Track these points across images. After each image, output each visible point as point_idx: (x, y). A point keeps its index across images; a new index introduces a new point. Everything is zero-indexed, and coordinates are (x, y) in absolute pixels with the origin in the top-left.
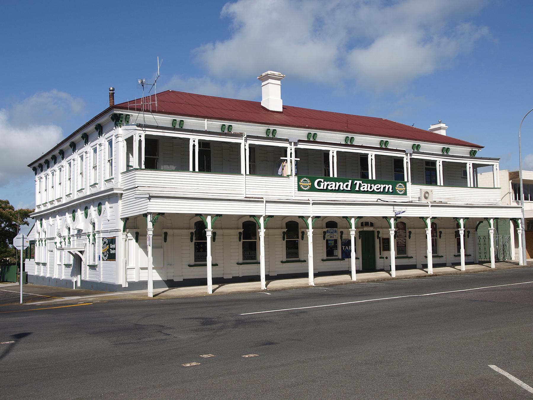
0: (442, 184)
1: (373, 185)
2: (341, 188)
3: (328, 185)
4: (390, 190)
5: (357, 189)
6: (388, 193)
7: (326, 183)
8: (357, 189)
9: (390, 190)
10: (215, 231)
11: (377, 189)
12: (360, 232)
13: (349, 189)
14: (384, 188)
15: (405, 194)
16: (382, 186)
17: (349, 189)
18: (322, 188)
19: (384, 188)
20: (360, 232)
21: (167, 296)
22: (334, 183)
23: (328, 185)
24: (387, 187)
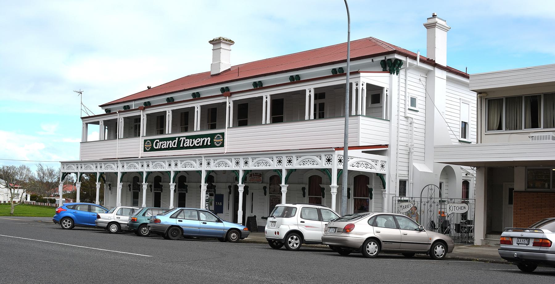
0: (365, 115)
1: (194, 140)
2: (171, 147)
3: (162, 144)
4: (209, 144)
5: (181, 146)
6: (207, 146)
7: (161, 143)
8: (181, 146)
9: (209, 144)
10: (247, 184)
11: (198, 143)
12: (379, 102)
13: (176, 146)
14: (204, 141)
15: (222, 145)
16: (202, 140)
17: (176, 146)
18: (157, 148)
19: (204, 141)
20: (379, 102)
21: (545, 257)
22: (165, 142)
23: (162, 144)
24: (206, 139)
